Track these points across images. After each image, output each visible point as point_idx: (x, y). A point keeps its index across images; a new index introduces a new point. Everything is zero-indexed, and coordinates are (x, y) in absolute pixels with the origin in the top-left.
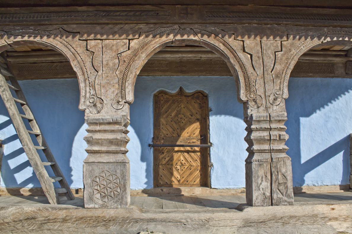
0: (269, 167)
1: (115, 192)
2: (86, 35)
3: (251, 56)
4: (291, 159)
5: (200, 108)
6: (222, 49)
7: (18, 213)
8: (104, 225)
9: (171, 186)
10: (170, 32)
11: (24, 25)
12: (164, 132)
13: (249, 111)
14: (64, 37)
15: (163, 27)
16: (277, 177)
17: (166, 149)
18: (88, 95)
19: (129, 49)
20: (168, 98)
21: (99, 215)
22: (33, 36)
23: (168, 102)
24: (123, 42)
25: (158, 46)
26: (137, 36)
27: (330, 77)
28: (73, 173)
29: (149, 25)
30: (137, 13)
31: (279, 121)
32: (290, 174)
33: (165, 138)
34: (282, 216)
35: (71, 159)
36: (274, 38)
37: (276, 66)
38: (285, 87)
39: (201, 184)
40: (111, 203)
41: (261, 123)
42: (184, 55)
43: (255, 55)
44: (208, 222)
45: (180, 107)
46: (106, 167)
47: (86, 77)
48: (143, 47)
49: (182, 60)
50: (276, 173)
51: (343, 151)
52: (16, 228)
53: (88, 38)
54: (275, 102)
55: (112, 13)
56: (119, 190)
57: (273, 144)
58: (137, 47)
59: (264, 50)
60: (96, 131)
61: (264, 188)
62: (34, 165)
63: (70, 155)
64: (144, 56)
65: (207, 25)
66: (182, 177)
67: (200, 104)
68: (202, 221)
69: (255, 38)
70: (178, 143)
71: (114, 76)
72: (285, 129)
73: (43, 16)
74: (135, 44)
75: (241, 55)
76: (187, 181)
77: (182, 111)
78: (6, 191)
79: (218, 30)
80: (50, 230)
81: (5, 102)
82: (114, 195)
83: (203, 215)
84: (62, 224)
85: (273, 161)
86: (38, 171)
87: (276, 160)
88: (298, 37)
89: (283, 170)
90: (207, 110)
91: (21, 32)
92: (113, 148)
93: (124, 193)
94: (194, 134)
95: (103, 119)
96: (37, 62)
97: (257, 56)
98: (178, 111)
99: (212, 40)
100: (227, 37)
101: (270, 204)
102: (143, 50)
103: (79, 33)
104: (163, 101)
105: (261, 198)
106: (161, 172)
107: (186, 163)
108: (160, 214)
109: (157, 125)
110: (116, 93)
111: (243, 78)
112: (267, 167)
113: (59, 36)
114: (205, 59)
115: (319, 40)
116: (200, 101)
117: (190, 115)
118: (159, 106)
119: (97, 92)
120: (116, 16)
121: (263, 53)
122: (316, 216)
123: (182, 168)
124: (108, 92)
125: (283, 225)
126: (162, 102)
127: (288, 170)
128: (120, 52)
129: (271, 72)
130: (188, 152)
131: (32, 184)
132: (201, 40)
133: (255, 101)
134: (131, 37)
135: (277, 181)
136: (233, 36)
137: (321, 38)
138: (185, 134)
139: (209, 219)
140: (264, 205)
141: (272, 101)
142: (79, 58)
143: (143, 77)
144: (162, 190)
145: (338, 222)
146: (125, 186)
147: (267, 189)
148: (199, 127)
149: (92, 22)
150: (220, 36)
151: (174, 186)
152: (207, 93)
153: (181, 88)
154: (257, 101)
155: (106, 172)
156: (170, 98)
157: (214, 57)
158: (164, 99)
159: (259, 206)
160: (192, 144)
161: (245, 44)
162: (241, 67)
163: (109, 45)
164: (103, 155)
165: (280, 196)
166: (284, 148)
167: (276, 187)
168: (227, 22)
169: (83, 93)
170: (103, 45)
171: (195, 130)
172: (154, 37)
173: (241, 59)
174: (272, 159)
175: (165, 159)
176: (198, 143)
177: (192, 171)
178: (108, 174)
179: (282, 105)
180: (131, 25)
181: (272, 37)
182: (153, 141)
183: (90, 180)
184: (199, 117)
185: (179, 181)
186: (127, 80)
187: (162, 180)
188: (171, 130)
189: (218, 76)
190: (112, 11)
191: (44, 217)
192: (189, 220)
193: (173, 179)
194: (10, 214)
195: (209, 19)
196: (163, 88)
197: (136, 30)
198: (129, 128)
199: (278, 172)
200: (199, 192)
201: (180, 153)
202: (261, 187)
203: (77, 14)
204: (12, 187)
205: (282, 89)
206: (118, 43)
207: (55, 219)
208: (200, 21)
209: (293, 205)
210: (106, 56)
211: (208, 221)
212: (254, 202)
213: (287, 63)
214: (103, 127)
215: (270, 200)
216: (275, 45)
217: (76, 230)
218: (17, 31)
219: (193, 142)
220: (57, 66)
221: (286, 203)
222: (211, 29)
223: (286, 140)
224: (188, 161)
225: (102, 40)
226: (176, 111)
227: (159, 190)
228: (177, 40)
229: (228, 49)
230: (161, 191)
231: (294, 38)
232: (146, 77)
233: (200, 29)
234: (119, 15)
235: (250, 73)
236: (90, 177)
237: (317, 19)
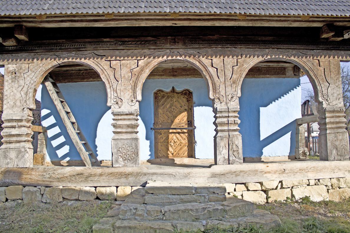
1: (131, 157)
2: (109, 58)
3: (217, 69)
4: (241, 136)
6: (198, 65)
7: (72, 171)
8: (126, 177)
9: (168, 157)
11: (69, 51)
12: (162, 119)
13: (215, 105)
14: (95, 59)
17: (163, 131)
18: (112, 97)
19: (138, 66)
20: (164, 95)
21: (122, 171)
22: (75, 58)
26: (143, 58)
27: (282, 77)
28: (97, 149)
29: (150, 50)
30: (143, 43)
31: (234, 111)
33: (162, 123)
34: (236, 171)
35: (96, 139)
36: (233, 57)
37: (233, 76)
40: (129, 164)
41: (222, 113)
42: (175, 64)
44: (189, 174)
46: (126, 142)
47: (111, 85)
48: (147, 65)
49: (174, 67)
50: (232, 144)
51: (291, 132)
52: (72, 180)
53: (111, 59)
54: (232, 99)
55: (126, 43)
56: (134, 156)
57: (230, 126)
58: (143, 65)
60: (118, 120)
62: (76, 143)
63: (95, 136)
65: (188, 49)
67: (187, 98)
68: (186, 174)
69: (220, 57)
70: (172, 127)
73: (81, 45)
75: (210, 69)
76: (179, 154)
77: (174, 104)
78: (51, 163)
79: (195, 52)
80: (92, 181)
81: (54, 101)
82: (131, 159)
83: (186, 170)
84: (99, 177)
86: (78, 147)
88: (248, 56)
89: (236, 143)
91: (66, 56)
92: (130, 130)
93: (137, 158)
95: (123, 112)
96: (68, 70)
101: (228, 163)
103: (105, 56)
105: (222, 159)
106: (160, 148)
107: (178, 141)
108: (160, 170)
109: (156, 114)
112: (226, 141)
113: (92, 58)
115: (263, 57)
119: (118, 95)
122: (257, 171)
123: (175, 145)
124: (126, 94)
125: (236, 176)
127: (239, 142)
129: (230, 80)
130: (179, 133)
131: (69, 157)
133: (219, 99)
134: (139, 58)
135: (233, 149)
136: (206, 56)
137: (264, 56)
138: (177, 121)
139: (190, 173)
142: (106, 73)
144: (161, 160)
145: (270, 174)
146: (137, 153)
149: (113, 48)
150: (197, 56)
151: (170, 158)
152: (192, 90)
153: (173, 87)
154: (221, 99)
155: (126, 145)
156: (166, 94)
159: (221, 165)
160: (182, 127)
162: (210, 77)
163: (125, 64)
164: (123, 134)
165: (234, 158)
166: (237, 128)
167: (232, 153)
168: (201, 47)
169: (109, 95)
170: (121, 64)
172: (154, 58)
174: (229, 135)
175: (163, 138)
176: (186, 127)
177: (182, 147)
178: (127, 146)
181: (231, 57)
182: (154, 126)
183: (116, 150)
184: (186, 108)
185: (173, 154)
186: (137, 86)
187: (160, 154)
188: (166, 117)
189: (200, 78)
190: (126, 41)
191: (88, 173)
192: (177, 174)
193: (169, 152)
194: (67, 171)
195: (189, 46)
196: (160, 87)
198: (139, 117)
199: (233, 144)
200: (187, 161)
201: (173, 134)
202: (222, 153)
203: (103, 44)
204: (55, 160)
206: (131, 63)
207: (95, 174)
208: (184, 47)
211: (189, 174)
212: (217, 162)
213: (241, 73)
214: (123, 117)
215: (228, 161)
216: (233, 61)
217: (108, 180)
218: (64, 55)
219: (183, 126)
220: (83, 73)
221: (238, 163)
225: (120, 60)
226: (170, 104)
227: (158, 160)
228: (169, 60)
230: (160, 161)
231: (246, 57)
234: (131, 44)
236: (116, 148)
237: (262, 44)
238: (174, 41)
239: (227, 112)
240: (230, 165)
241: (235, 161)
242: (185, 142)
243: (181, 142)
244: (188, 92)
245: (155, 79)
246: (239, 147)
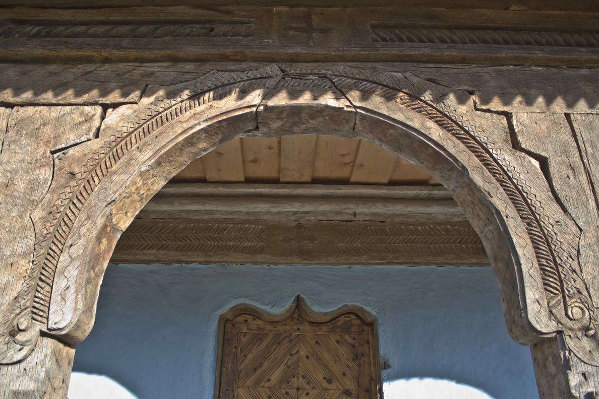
5: (354, 360)
6: (435, 137)
10: (250, 85)
15: (226, 71)
19: (97, 135)
20: (263, 329)
23: (261, 339)
24: (82, 114)
25: (202, 129)
29: (180, 65)
30: (144, 29)
43: (558, 159)
45: (297, 355)
49: (303, 222)
58: (126, 128)
59: (587, 145)
64: (145, 158)
67: (354, 346)
71: (24, 227)
74: (123, 118)
75: (506, 157)
79: (415, 80)
90: (375, 366)
97: (564, 161)
98: (288, 367)
99: (398, 111)
100: (451, 99)
102: (148, 138)
104: (248, 336)
110: (15, 294)
111: (529, 241)
114: (366, 219)
116: (354, 339)
117: (325, 378)
118: (234, 350)
120: (75, 35)
121: (584, 154)
126: (244, 340)
128: (63, 146)
132: (359, 110)
134: (115, 97)
143: (193, 265)
150: (427, 96)
152: (374, 313)
153: (298, 300)
156: (269, 327)
157: (390, 213)
158: (252, 330)
161: (515, 122)
172: (196, 96)
173: (510, 174)
180: (121, 66)
189: (402, 267)
196: (246, 297)
197: (135, 78)
210: (10, 157)
222: (392, 77)
226: (283, 367)
229: (459, 138)
232: (200, 265)
233: (353, 78)
234: (84, 35)
235: (552, 222)
238: (303, 25)
244: (359, 322)
245: (228, 263)
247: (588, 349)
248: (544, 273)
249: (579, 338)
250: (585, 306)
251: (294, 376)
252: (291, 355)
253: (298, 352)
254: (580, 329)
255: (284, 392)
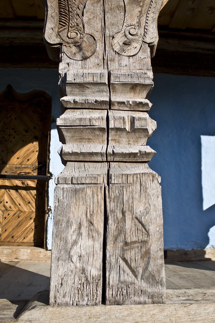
0: (100, 197)
16: (121, 224)
32: (156, 219)
38: (151, 22)
39: (36, 242)
41: (87, 91)
50: (120, 216)
54: (126, 48)
61: (83, 253)
66: (5, 230)
72: (147, 104)
85: (113, 182)
87: (120, 180)
89: (139, 209)
94: (28, 160)
98: (5, 124)
101: (100, 298)
105: (73, 281)
107: (12, 206)
112: (94, 199)
117: (24, 130)
127: (152, 207)
130: (16, 188)
135: (121, 238)
138: (14, 161)
140: (81, 303)
141: (118, 47)
147: (91, 259)
148: (38, 149)
153: (9, 87)
154: (84, 45)
159: (67, 304)
165: (129, 277)
167: (118, 252)
171: (30, 153)
179: (142, 57)
199: (123, 213)
201: (3, 190)
202: (75, 251)
205: (143, 24)
209: (163, 303)
223: (150, 132)
224: (16, 204)
239: (106, 88)
240: (108, 307)
241: (131, 290)
242: (30, 209)
243: (21, 209)
246: (152, 228)
247: (74, 52)
248: (60, 15)
249: (70, 47)
250: (79, 32)
251: (7, 129)
252: (7, 118)
253: (11, 116)
254: (72, 43)
255: (2, 136)
